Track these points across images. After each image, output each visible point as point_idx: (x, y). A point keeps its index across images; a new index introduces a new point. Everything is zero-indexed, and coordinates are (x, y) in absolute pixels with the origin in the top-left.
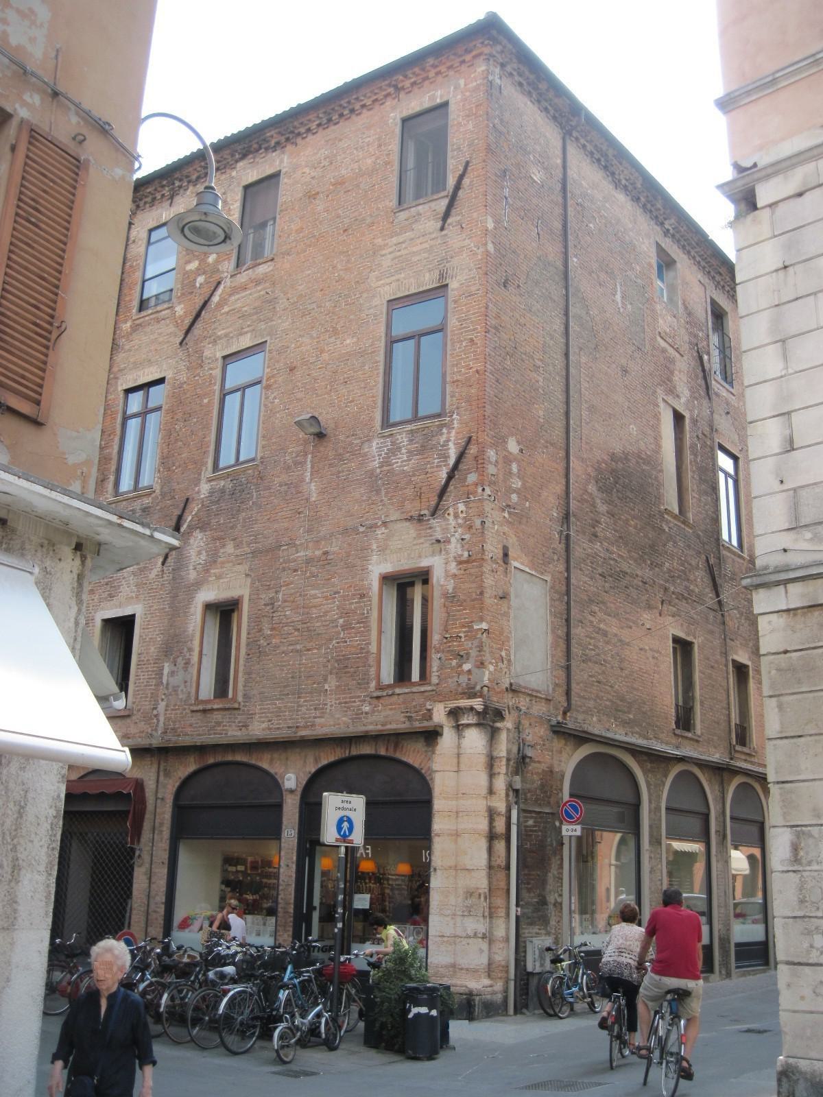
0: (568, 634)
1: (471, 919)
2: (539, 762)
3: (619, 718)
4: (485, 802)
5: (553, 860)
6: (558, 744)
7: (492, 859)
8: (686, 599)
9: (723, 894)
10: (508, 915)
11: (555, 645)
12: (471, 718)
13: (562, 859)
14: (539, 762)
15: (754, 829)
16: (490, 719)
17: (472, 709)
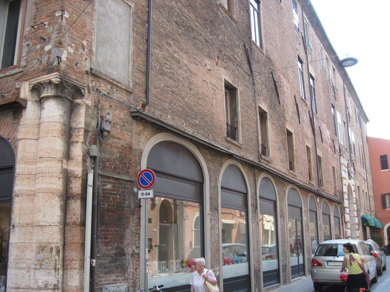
0: (148, 51)
1: (42, 272)
2: (118, 138)
3: (189, 121)
4: (60, 165)
5: (131, 219)
6: (137, 127)
7: (68, 216)
8: (233, 62)
9: (256, 243)
10: (82, 266)
11: (136, 54)
12: (49, 91)
13: (140, 218)
14: (118, 138)
15: (271, 205)
16: (69, 93)
17: (50, 83)
